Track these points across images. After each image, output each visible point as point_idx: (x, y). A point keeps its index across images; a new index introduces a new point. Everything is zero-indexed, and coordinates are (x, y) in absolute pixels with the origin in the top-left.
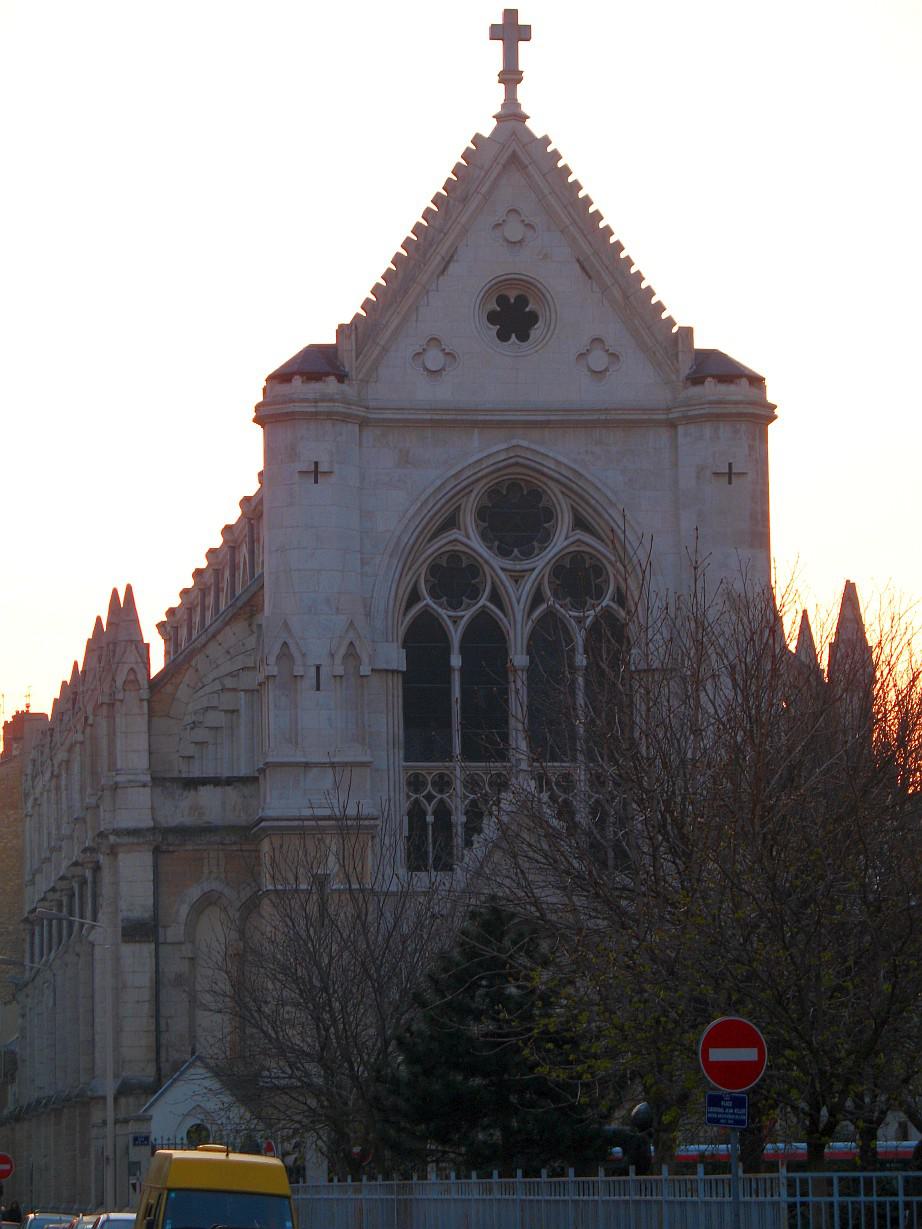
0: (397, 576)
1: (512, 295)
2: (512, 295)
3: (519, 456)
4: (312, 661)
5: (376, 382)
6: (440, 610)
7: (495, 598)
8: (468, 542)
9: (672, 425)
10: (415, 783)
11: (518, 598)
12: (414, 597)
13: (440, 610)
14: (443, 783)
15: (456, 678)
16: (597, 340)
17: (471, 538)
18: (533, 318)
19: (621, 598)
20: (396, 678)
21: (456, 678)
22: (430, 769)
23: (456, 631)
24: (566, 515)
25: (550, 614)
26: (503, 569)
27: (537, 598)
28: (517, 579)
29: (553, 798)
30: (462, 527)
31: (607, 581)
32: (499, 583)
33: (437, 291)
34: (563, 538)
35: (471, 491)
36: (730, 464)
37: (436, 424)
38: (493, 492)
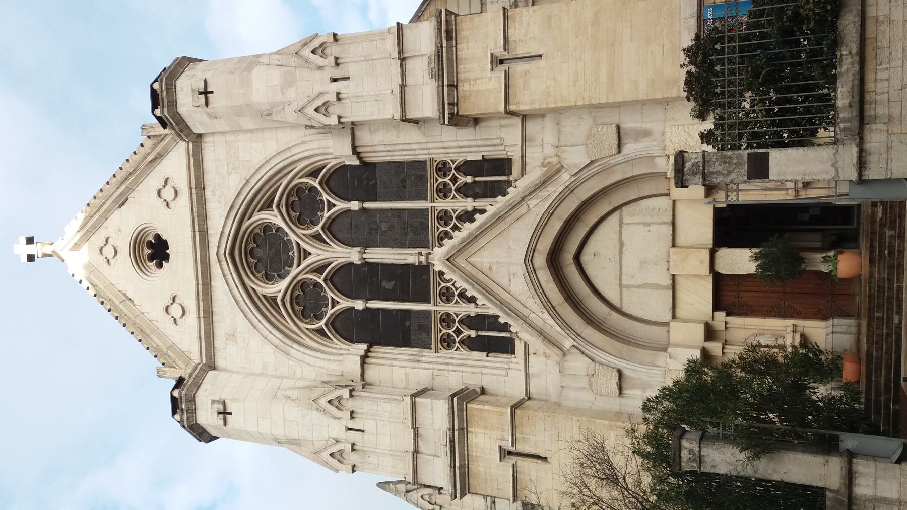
0: (302, 349)
1: (147, 251)
2: (147, 251)
3: (225, 254)
4: (342, 434)
5: (191, 353)
6: (328, 315)
7: (319, 270)
8: (282, 291)
9: (619, 106)
10: (447, 342)
11: (318, 254)
12: (320, 332)
13: (328, 315)
14: (447, 320)
15: (374, 304)
16: (159, 193)
17: (278, 288)
18: (158, 237)
19: (314, 174)
20: (373, 361)
21: (374, 304)
22: (438, 331)
23: (342, 304)
24: (261, 217)
25: (329, 227)
26: (299, 265)
27: (317, 237)
28: (307, 254)
29: (455, 228)
30: (276, 295)
31: (306, 183)
32: (555, 178)
33: (141, 305)
34: (273, 217)
35: (254, 289)
36: (205, 81)
37: (530, 194)
38: (255, 269)
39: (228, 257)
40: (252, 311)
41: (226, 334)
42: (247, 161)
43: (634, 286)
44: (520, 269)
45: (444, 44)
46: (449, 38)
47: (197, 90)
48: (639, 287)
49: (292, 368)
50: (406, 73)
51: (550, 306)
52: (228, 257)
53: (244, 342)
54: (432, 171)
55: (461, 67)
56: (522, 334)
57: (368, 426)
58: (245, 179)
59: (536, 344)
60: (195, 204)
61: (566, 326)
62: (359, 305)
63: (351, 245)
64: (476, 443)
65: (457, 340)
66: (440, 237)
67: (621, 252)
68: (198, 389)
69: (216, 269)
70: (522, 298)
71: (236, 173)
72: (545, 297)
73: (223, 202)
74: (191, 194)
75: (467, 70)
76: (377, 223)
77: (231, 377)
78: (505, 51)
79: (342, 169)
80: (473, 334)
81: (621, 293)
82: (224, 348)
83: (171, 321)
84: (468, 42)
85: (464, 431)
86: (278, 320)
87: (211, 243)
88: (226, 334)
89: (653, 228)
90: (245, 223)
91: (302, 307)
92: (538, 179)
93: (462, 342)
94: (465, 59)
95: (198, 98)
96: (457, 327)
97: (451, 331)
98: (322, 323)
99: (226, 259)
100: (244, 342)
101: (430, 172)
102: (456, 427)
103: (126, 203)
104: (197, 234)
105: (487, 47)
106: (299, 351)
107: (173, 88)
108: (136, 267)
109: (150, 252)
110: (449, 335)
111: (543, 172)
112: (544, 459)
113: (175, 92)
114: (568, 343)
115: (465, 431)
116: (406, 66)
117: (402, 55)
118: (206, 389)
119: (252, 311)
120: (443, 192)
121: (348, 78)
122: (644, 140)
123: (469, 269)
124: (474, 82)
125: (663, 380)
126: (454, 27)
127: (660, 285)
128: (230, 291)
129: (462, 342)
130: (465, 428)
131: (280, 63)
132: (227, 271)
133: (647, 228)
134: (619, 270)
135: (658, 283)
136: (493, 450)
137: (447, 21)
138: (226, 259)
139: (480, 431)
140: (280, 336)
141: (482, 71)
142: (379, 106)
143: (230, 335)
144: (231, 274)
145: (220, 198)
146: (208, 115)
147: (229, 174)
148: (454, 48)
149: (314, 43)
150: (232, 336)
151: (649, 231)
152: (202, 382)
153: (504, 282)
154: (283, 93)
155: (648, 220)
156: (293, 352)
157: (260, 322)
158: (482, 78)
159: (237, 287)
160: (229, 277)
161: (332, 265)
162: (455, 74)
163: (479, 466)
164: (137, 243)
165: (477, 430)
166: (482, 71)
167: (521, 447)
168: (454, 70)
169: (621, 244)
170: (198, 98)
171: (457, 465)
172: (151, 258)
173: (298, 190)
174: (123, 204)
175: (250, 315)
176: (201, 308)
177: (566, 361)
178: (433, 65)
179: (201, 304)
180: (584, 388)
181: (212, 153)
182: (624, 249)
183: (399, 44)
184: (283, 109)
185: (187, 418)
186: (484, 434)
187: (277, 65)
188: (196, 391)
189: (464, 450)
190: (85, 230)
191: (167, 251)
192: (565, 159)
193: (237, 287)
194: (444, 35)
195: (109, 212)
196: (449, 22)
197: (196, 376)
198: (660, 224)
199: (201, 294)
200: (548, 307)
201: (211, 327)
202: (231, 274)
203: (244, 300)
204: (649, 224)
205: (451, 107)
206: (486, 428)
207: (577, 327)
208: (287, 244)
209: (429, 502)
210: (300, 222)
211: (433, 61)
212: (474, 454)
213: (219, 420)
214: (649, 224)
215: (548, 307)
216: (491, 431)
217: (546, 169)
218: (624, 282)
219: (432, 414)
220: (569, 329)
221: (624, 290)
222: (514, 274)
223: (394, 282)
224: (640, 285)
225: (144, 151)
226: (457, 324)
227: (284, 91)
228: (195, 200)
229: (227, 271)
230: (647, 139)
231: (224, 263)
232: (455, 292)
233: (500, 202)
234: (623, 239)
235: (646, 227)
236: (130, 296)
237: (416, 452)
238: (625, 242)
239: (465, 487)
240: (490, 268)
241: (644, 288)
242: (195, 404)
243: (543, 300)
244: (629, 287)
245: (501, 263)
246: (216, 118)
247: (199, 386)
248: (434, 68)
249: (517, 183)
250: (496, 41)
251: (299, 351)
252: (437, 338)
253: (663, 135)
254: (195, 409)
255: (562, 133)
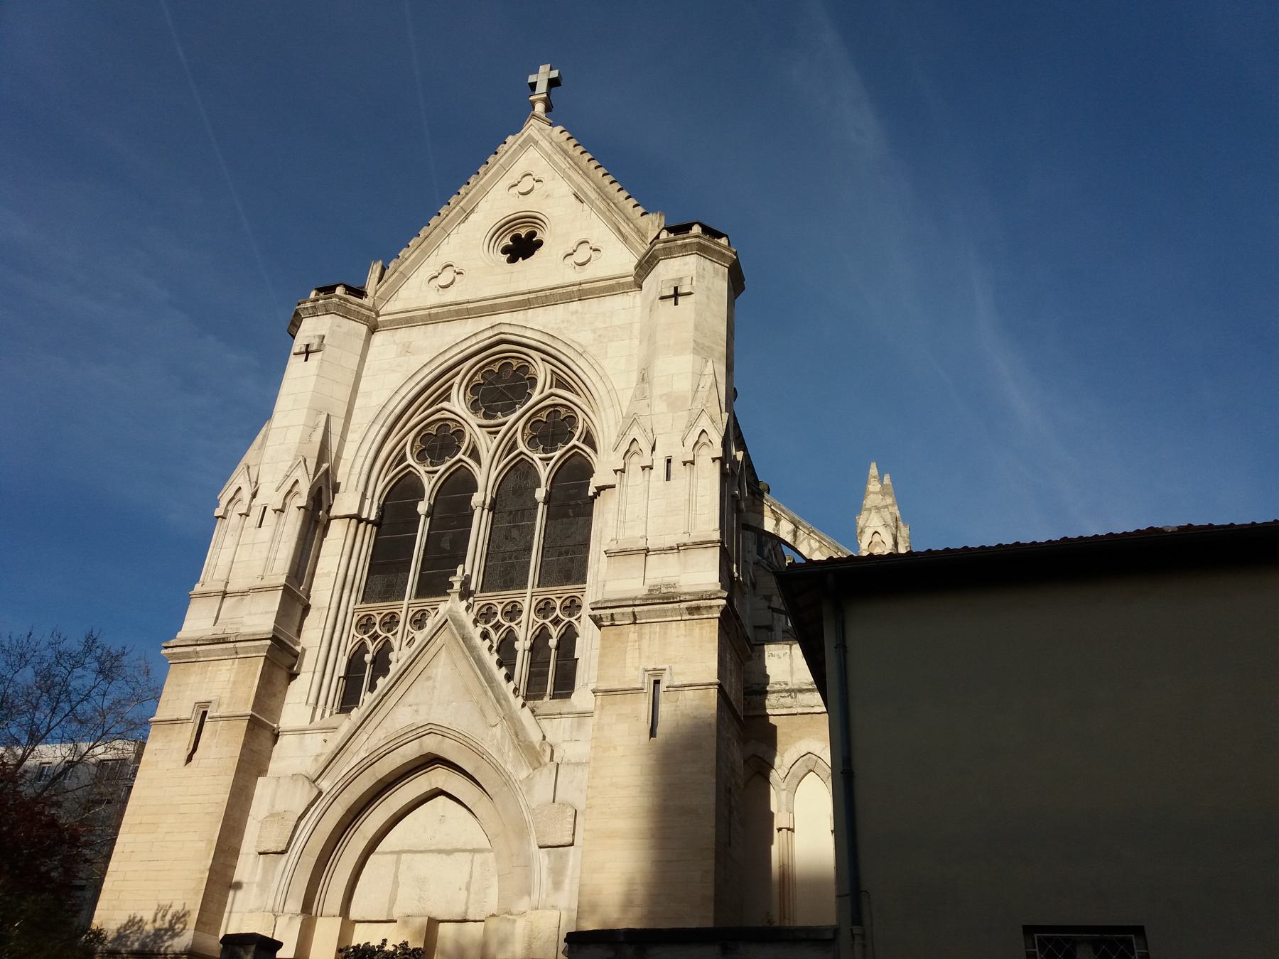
0: (379, 438)
10: (365, 624)
22: (378, 610)
26: (480, 426)
39: (497, 337)
40: (431, 372)
41: (410, 343)
42: (607, 352)
43: (397, 868)
44: (420, 720)
45: (683, 605)
46: (692, 610)
47: (681, 284)
48: (396, 877)
49: (359, 428)
50: (663, 555)
51: (373, 761)
52: (497, 337)
53: (398, 366)
54: (570, 591)
55: (657, 627)
56: (346, 723)
57: (266, 531)
58: (584, 351)
59: (336, 739)
60: (561, 291)
61: (347, 782)
62: (422, 507)
63: (382, 509)
64: (221, 670)
65: (547, 621)
66: (492, 606)
67: (440, 851)
68: (342, 316)
69: (486, 322)
70: (386, 724)
71: (594, 340)
72: (385, 753)
73: (562, 326)
74: (574, 285)
75: (652, 637)
76: (522, 521)
77: (356, 354)
78: (667, 687)
79: (588, 471)
80: (553, 643)
81: (392, 852)
82: (394, 341)
83: (434, 272)
84: (686, 636)
85: (233, 654)
86: (421, 405)
87: (517, 314)
88: (410, 343)
89: (464, 893)
90: (537, 355)
91: (545, 420)
92: (525, 738)
93: (544, 628)
94: (665, 633)
95: (670, 287)
96: (563, 620)
97: (558, 611)
98: (522, 447)
99: (495, 335)
100: (398, 366)
101: (569, 590)
102: (238, 645)
103: (578, 201)
104: (526, 297)
105: (676, 663)
106: (377, 435)
107: (688, 251)
108: (504, 221)
109: (523, 236)
110: (554, 609)
111: (535, 743)
112: (189, 759)
113: (683, 256)
114: (325, 785)
115: (235, 657)
116: (671, 555)
117: (683, 548)
118: (340, 327)
119: (431, 372)
120: (544, 609)
121: (668, 478)
122: (550, 880)
123: (432, 649)
124: (637, 647)
125: (267, 910)
126: (704, 616)
127: (394, 903)
128: (457, 344)
129: (544, 628)
130: (238, 656)
131: (700, 389)
132: (480, 337)
133: (463, 887)
134: (419, 849)
135: (397, 902)
136: (210, 692)
137: (711, 607)
138: (495, 335)
139: (233, 675)
140: (397, 411)
141: (649, 657)
142: (631, 521)
143: (409, 347)
144: (477, 343)
145: (568, 321)
146: (654, 301)
147: (594, 331)
148: (679, 618)
149: (714, 433)
150: (407, 350)
151: (460, 889)
152: (352, 320)
153: (410, 698)
154: (661, 396)
155: (473, 888)
156: (376, 427)
157: (417, 384)
158: (640, 658)
159: (462, 351)
160: (474, 340)
161: (592, 454)
162: (648, 621)
163: (197, 675)
164: (532, 220)
165: (234, 671)
166: (649, 657)
167: (208, 725)
168: (653, 618)
169: (449, 852)
170: (670, 287)
171: (198, 648)
172: (516, 238)
173: (572, 420)
174: (577, 197)
175: (426, 371)
176: (440, 310)
177: (303, 783)
178: (664, 590)
179: (446, 309)
180: (273, 807)
181: (628, 306)
182: (443, 856)
183: (695, 544)
184: (645, 397)
185: (307, 308)
186: (229, 681)
187: (699, 385)
188: (339, 315)
189: (215, 656)
190: (550, 153)
191: (520, 259)
192: (541, 775)
193: (462, 351)
194: (694, 603)
195: (569, 180)
196: (710, 611)
197: (358, 312)
198: (467, 903)
199: (457, 307)
200: (372, 757)
201: (420, 324)
202: (477, 343)
203: (446, 361)
204: (468, 889)
205: (609, 618)
206: (234, 683)
207: (345, 796)
208: (510, 409)
209: (871, 542)
210: (534, 424)
211: (669, 590)
212: (210, 668)
213: (299, 346)
214: (468, 889)
215: (372, 757)
216: (229, 690)
217: (538, 746)
218: (404, 856)
219: (262, 613)
220: (343, 786)
221: (395, 857)
222: (417, 711)
223: (449, 548)
224: (397, 877)
225: (634, 217)
226: (567, 620)
227: (664, 398)
228: (565, 290)
229: (480, 337)
230: (550, 886)
231: (491, 333)
232: (548, 620)
233: (507, 687)
234: (456, 854)
235: (465, 884)
236: (470, 218)
237: (647, 551)
238: (451, 856)
239: (176, 658)
240: (429, 678)
241: (394, 883)
242: (323, 315)
243: (381, 750)
244: (398, 862)
245: (433, 693)
246: (651, 311)
247: (346, 317)
248: (660, 592)
249: (527, 710)
250: (681, 674)
251: (377, 435)
252: (372, 609)
253: (553, 906)
254: (318, 316)
255: (576, 768)
